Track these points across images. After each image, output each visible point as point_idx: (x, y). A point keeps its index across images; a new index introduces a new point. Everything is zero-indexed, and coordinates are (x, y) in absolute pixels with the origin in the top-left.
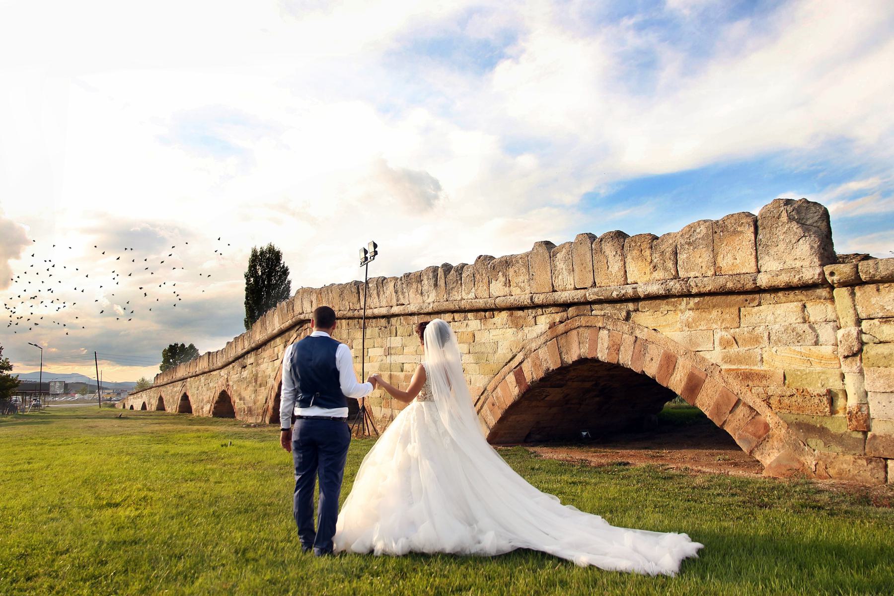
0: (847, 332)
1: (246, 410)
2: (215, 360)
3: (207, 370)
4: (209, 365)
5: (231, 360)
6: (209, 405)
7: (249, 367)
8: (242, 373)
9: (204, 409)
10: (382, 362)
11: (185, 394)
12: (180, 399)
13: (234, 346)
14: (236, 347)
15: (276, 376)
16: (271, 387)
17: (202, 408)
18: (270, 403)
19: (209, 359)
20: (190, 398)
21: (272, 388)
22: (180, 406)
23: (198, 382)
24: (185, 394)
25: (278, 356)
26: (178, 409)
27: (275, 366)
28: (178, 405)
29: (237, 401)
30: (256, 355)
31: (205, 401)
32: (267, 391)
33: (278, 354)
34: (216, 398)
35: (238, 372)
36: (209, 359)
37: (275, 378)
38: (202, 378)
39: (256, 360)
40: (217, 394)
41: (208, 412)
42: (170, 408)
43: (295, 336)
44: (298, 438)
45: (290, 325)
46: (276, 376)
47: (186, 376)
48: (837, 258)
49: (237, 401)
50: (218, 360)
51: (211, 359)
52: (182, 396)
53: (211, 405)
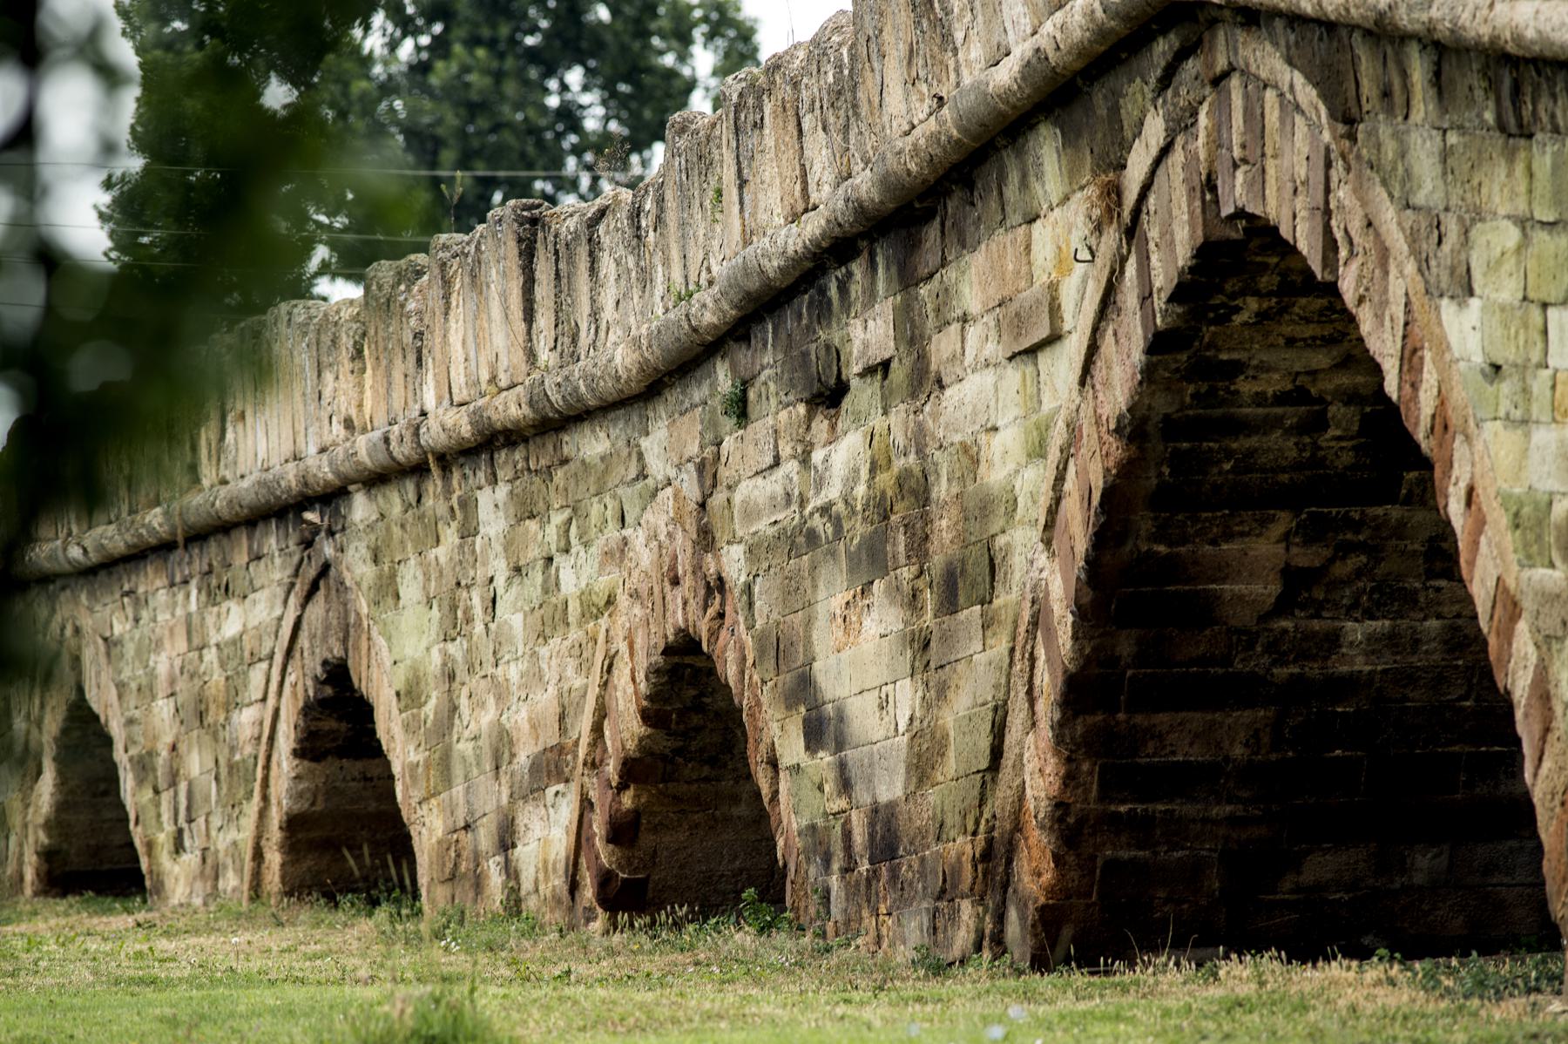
0: (823, 492)
1: (859, 838)
2: (585, 309)
3: (511, 409)
4: (531, 356)
5: (709, 318)
6: (566, 811)
7: (862, 394)
8: (817, 456)
9: (527, 854)
10: (500, 505)
11: (337, 675)
12: (286, 740)
13: (729, 174)
14: (742, 183)
15: (1058, 500)
16: (1026, 615)
17: (506, 841)
18: (1031, 766)
19: (529, 315)
20: (390, 725)
21: (1034, 623)
22: (293, 824)
23: (450, 536)
24: (337, 675)
25: (1055, 310)
26: (274, 858)
27: (1048, 405)
28: (276, 818)
29: (792, 748)
30: (908, 280)
31: (523, 758)
32: (1000, 646)
33: (1053, 288)
34: (627, 729)
35: (786, 450)
36: (529, 315)
37: (1049, 526)
38: (485, 498)
39: (912, 335)
40: (628, 695)
41: (559, 882)
42: (191, 859)
43: (1155, 129)
44: (19, 606)
45: (1101, 33)
46: (1058, 500)
47: (323, 471)
48: (807, 402)
49: (792, 748)
50: (608, 297)
51: (544, 291)
52: (308, 710)
53: (586, 805)
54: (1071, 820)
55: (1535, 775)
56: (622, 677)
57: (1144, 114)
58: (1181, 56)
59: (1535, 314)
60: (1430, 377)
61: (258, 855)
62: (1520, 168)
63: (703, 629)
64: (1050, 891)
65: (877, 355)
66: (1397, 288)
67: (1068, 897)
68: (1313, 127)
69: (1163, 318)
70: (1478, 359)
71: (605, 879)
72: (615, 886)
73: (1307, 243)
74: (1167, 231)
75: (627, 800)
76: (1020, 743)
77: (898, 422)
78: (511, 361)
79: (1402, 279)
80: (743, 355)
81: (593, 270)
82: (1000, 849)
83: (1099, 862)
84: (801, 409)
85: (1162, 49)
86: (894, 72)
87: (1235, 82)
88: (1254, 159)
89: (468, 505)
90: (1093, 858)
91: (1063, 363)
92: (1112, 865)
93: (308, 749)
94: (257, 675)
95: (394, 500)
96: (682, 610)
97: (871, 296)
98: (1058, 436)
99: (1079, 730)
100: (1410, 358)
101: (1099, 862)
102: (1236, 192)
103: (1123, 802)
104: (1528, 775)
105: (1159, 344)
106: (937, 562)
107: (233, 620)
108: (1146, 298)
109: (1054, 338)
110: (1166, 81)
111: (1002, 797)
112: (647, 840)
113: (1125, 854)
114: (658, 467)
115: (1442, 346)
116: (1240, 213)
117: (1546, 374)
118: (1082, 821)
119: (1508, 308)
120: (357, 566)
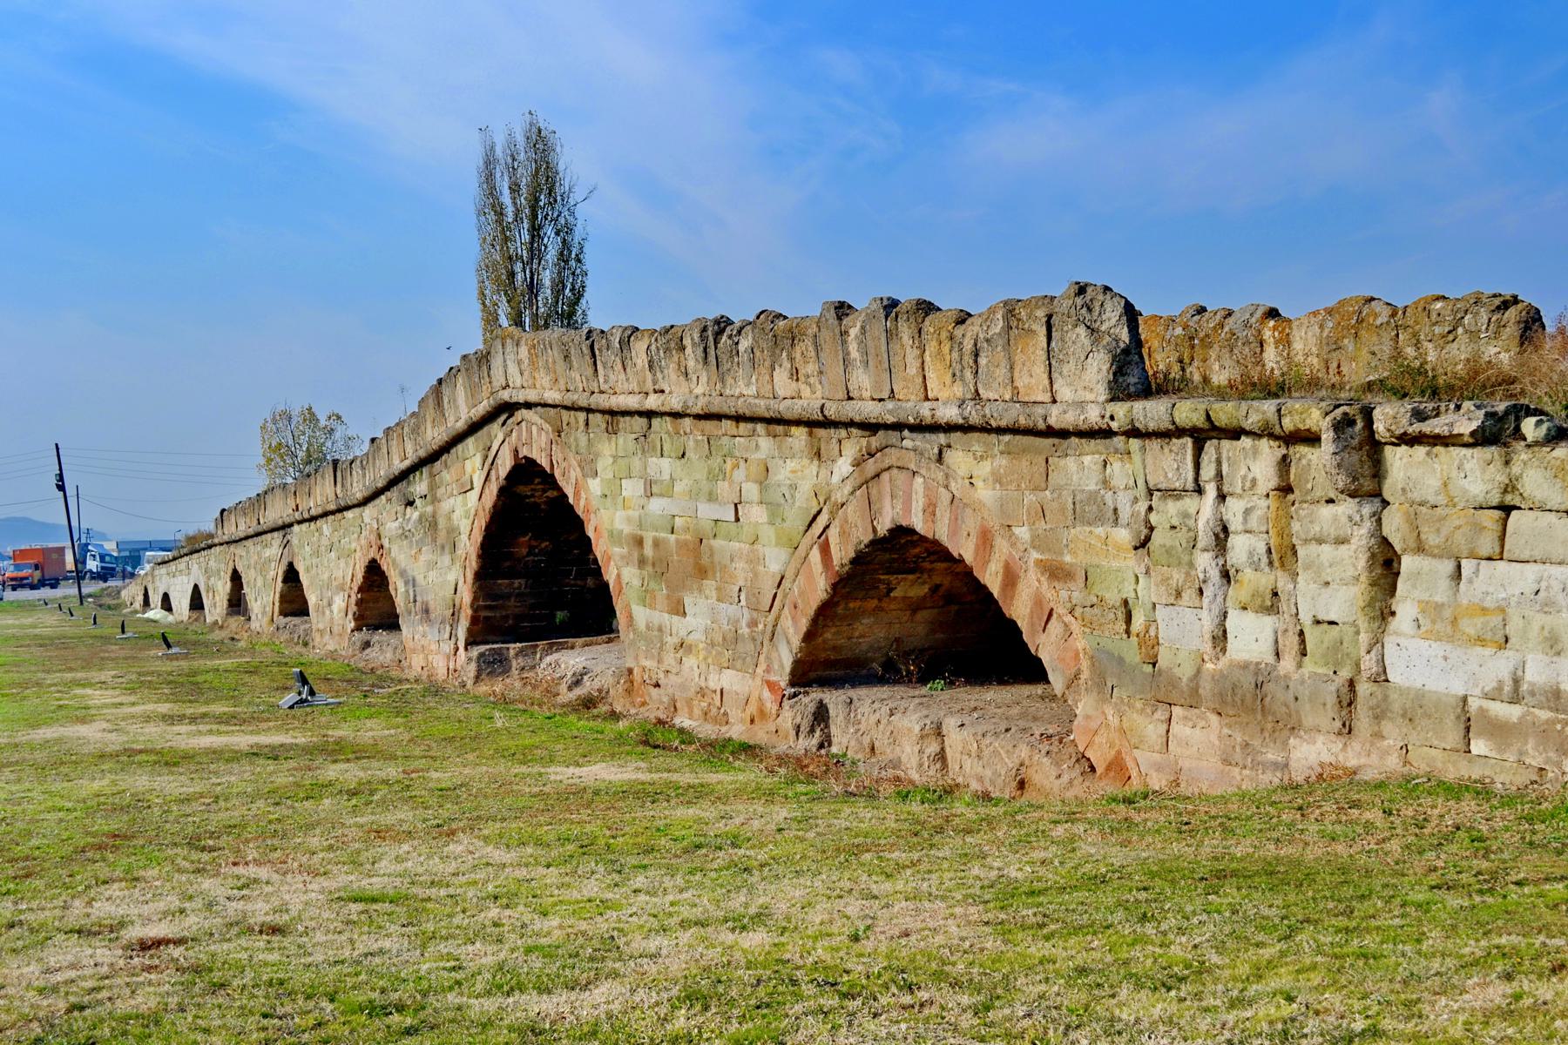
11: (291, 565)
12: (280, 579)
24: (291, 565)
26: (277, 604)
38: (325, 526)
39: (433, 487)
56: (357, 566)
57: (975, 559)
58: (508, 418)
59: (618, 482)
60: (583, 495)
62: (613, 444)
63: (378, 558)
65: (423, 493)
66: (573, 475)
68: (547, 433)
70: (599, 493)
73: (545, 463)
74: (504, 462)
77: (429, 509)
78: (332, 497)
79: (575, 473)
80: (388, 493)
85: (503, 417)
86: (429, 425)
87: (524, 424)
88: (529, 443)
89: (321, 528)
91: (474, 495)
93: (285, 581)
94: (273, 564)
95: (304, 526)
96: (373, 554)
97: (421, 480)
98: (473, 512)
100: (577, 494)
102: (524, 452)
105: (502, 491)
106: (1283, 946)
107: (268, 553)
108: (498, 478)
109: (472, 488)
110: (503, 424)
114: (367, 520)
115: (587, 490)
116: (525, 457)
119: (1252, 667)
120: (295, 541)
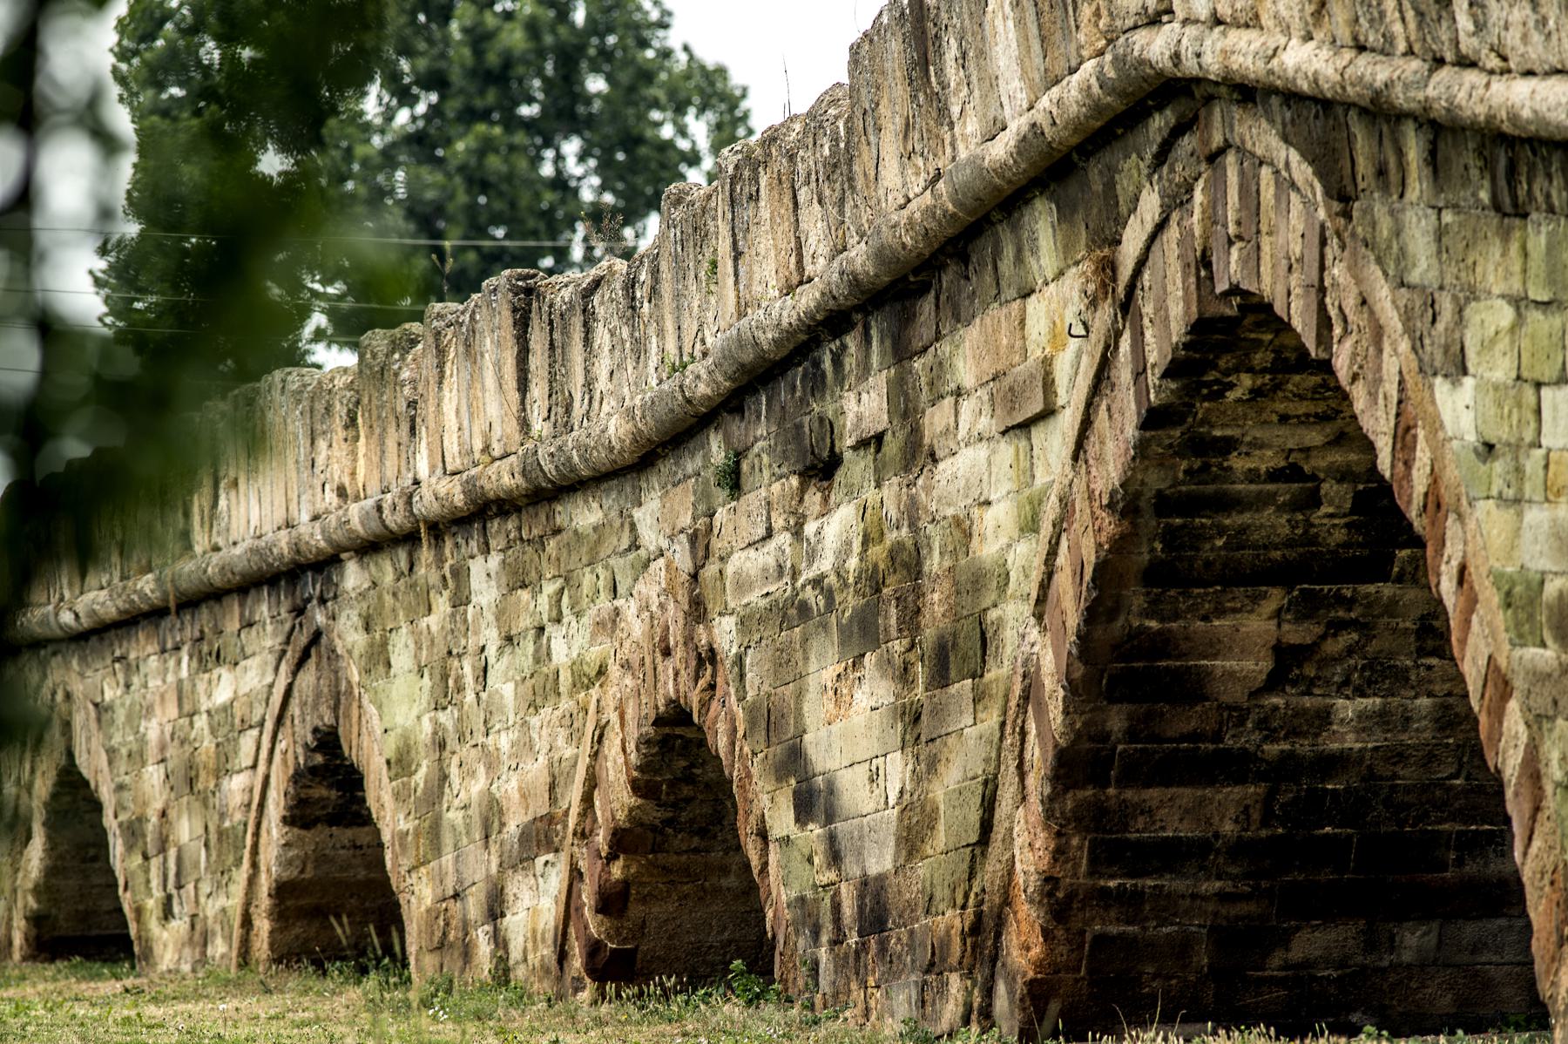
26: (263, 926)
28: (265, 884)
54: (1060, 895)
55: (1525, 854)
61: (247, 922)
64: (1038, 965)
67: (1057, 972)
69: (1157, 393)
71: (594, 950)
72: (603, 957)
75: (617, 871)
76: (1010, 817)
81: (587, 341)
82: (989, 923)
83: (1088, 937)
84: (794, 481)
90: (1082, 933)
92: (1101, 940)
99: (1069, 805)
101: (1088, 937)
103: (1112, 877)
104: (1517, 854)
111: (991, 871)
112: (635, 911)
113: (1114, 929)
117: (1538, 454)
118: (1071, 896)
